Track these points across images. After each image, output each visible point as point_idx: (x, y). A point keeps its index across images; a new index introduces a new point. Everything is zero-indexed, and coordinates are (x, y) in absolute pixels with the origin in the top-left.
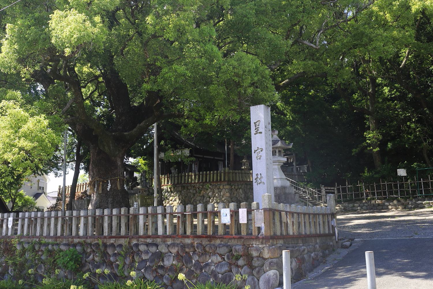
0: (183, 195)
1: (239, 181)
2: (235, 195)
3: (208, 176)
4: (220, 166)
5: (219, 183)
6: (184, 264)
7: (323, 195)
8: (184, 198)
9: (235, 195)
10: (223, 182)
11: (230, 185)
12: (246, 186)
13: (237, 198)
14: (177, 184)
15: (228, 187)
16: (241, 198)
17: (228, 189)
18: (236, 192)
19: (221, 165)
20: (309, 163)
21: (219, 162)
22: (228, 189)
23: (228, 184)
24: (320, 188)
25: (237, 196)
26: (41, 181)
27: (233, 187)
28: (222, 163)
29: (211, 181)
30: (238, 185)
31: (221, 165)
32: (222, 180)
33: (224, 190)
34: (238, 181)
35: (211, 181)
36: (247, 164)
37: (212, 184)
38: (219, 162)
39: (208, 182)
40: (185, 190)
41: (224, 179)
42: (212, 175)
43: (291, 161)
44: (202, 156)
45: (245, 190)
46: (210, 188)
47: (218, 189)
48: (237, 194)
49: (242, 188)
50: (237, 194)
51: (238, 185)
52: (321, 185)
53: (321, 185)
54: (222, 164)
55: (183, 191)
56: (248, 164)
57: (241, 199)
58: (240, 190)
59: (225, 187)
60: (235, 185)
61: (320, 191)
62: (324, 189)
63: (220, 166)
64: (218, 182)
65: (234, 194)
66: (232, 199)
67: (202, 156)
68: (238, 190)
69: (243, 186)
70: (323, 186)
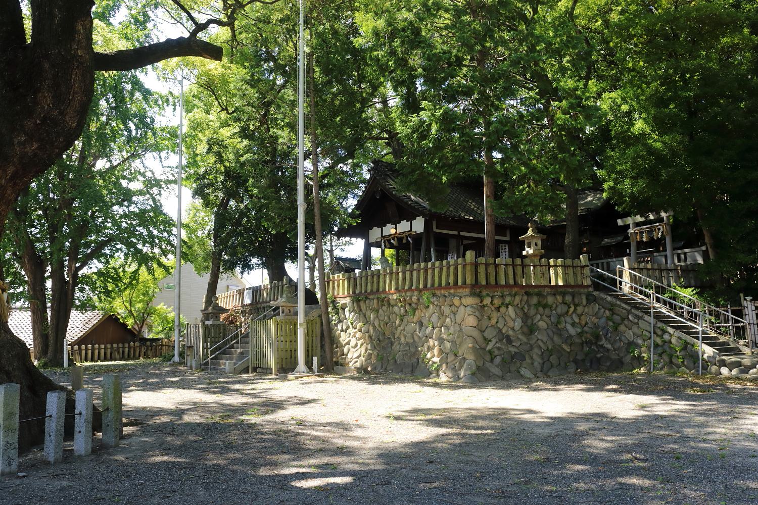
0: (381, 318)
1: (507, 285)
2: (493, 321)
3: (430, 272)
4: (504, 254)
5: (452, 291)
6: (651, 337)
7: (749, 324)
8: (382, 327)
9: (493, 321)
10: (460, 287)
11: (480, 296)
12: (525, 298)
13: (500, 330)
14: (369, 294)
15: (469, 301)
16: (513, 329)
17: (471, 306)
18: (495, 315)
19: (505, 252)
20: (707, 240)
21: (501, 245)
22: (471, 306)
23: (472, 294)
24: (740, 305)
25: (500, 325)
26: (230, 287)
27: (487, 301)
28: (507, 247)
29: (436, 285)
30: (502, 297)
31: (505, 252)
32: (460, 283)
33: (462, 308)
34: (502, 287)
35: (436, 285)
36: (536, 244)
37: (438, 292)
38: (501, 245)
39: (428, 290)
40: (385, 308)
41: (464, 283)
42: (437, 270)
43: (659, 236)
44: (456, 233)
45: (522, 309)
46: (433, 304)
47: (451, 306)
48: (501, 319)
49: (515, 303)
50: (501, 319)
51: (502, 297)
52: (742, 295)
53: (742, 295)
54: (507, 250)
55: (380, 310)
56: (539, 243)
57: (511, 333)
58: (507, 308)
59: (463, 301)
60: (492, 297)
61: (739, 313)
62: (754, 308)
63: (504, 254)
64: (451, 288)
65: (490, 318)
66: (482, 332)
67: (456, 233)
68: (503, 309)
69: (518, 299)
70: (749, 298)
